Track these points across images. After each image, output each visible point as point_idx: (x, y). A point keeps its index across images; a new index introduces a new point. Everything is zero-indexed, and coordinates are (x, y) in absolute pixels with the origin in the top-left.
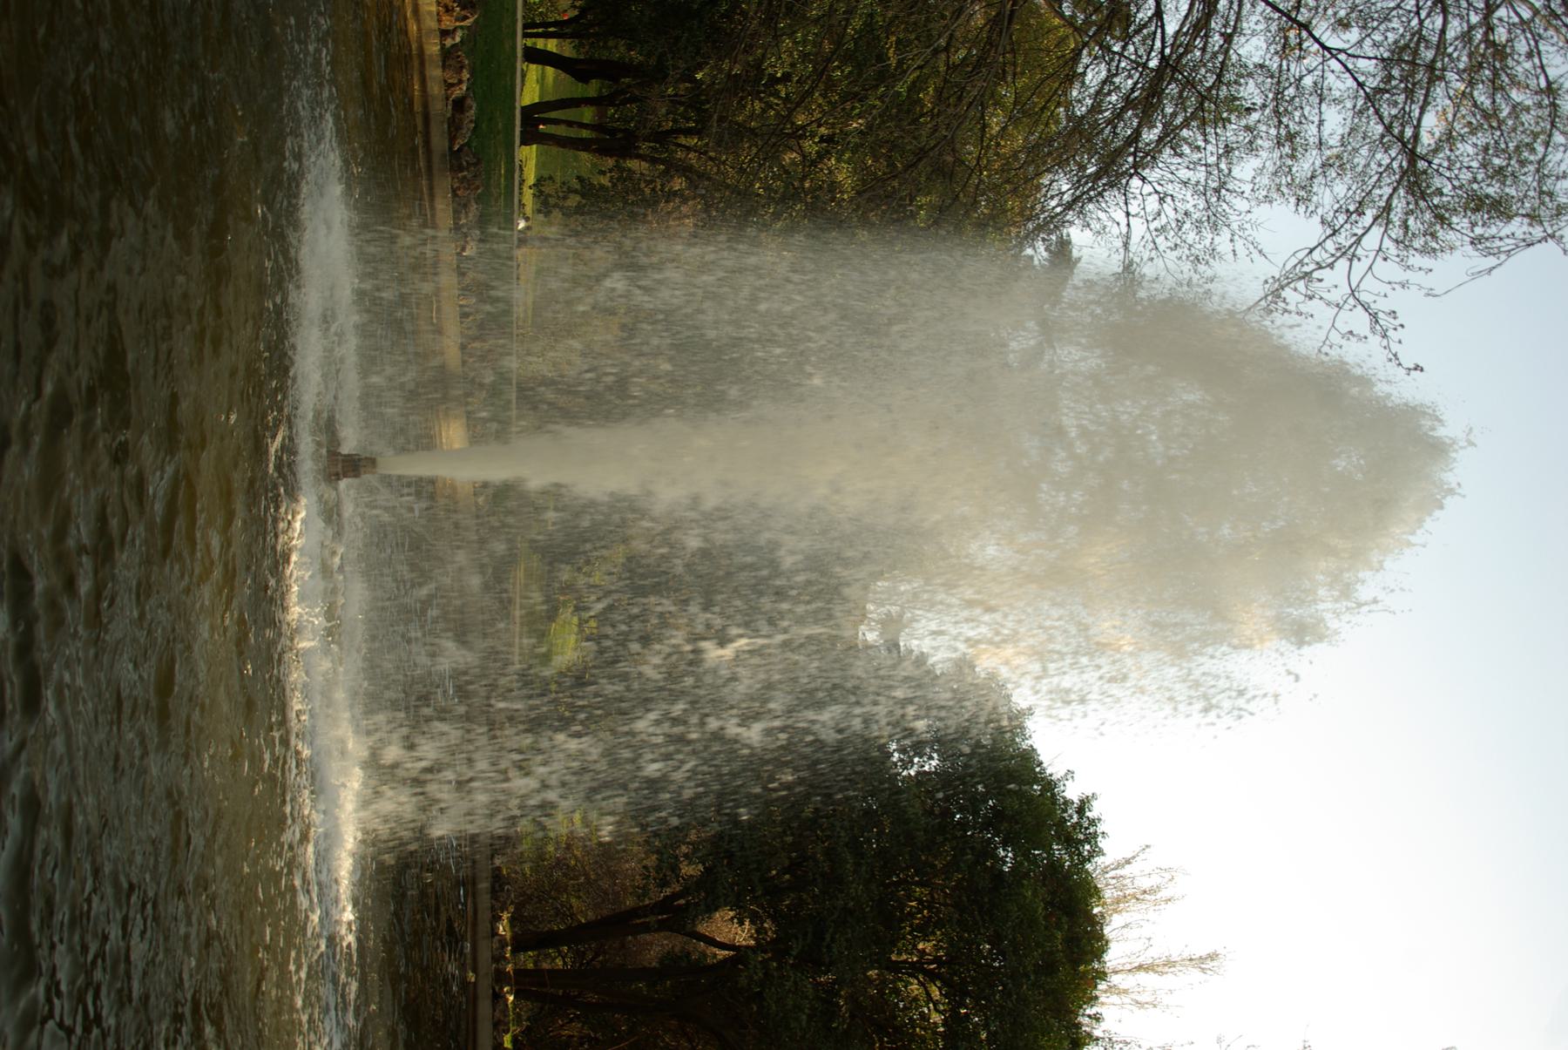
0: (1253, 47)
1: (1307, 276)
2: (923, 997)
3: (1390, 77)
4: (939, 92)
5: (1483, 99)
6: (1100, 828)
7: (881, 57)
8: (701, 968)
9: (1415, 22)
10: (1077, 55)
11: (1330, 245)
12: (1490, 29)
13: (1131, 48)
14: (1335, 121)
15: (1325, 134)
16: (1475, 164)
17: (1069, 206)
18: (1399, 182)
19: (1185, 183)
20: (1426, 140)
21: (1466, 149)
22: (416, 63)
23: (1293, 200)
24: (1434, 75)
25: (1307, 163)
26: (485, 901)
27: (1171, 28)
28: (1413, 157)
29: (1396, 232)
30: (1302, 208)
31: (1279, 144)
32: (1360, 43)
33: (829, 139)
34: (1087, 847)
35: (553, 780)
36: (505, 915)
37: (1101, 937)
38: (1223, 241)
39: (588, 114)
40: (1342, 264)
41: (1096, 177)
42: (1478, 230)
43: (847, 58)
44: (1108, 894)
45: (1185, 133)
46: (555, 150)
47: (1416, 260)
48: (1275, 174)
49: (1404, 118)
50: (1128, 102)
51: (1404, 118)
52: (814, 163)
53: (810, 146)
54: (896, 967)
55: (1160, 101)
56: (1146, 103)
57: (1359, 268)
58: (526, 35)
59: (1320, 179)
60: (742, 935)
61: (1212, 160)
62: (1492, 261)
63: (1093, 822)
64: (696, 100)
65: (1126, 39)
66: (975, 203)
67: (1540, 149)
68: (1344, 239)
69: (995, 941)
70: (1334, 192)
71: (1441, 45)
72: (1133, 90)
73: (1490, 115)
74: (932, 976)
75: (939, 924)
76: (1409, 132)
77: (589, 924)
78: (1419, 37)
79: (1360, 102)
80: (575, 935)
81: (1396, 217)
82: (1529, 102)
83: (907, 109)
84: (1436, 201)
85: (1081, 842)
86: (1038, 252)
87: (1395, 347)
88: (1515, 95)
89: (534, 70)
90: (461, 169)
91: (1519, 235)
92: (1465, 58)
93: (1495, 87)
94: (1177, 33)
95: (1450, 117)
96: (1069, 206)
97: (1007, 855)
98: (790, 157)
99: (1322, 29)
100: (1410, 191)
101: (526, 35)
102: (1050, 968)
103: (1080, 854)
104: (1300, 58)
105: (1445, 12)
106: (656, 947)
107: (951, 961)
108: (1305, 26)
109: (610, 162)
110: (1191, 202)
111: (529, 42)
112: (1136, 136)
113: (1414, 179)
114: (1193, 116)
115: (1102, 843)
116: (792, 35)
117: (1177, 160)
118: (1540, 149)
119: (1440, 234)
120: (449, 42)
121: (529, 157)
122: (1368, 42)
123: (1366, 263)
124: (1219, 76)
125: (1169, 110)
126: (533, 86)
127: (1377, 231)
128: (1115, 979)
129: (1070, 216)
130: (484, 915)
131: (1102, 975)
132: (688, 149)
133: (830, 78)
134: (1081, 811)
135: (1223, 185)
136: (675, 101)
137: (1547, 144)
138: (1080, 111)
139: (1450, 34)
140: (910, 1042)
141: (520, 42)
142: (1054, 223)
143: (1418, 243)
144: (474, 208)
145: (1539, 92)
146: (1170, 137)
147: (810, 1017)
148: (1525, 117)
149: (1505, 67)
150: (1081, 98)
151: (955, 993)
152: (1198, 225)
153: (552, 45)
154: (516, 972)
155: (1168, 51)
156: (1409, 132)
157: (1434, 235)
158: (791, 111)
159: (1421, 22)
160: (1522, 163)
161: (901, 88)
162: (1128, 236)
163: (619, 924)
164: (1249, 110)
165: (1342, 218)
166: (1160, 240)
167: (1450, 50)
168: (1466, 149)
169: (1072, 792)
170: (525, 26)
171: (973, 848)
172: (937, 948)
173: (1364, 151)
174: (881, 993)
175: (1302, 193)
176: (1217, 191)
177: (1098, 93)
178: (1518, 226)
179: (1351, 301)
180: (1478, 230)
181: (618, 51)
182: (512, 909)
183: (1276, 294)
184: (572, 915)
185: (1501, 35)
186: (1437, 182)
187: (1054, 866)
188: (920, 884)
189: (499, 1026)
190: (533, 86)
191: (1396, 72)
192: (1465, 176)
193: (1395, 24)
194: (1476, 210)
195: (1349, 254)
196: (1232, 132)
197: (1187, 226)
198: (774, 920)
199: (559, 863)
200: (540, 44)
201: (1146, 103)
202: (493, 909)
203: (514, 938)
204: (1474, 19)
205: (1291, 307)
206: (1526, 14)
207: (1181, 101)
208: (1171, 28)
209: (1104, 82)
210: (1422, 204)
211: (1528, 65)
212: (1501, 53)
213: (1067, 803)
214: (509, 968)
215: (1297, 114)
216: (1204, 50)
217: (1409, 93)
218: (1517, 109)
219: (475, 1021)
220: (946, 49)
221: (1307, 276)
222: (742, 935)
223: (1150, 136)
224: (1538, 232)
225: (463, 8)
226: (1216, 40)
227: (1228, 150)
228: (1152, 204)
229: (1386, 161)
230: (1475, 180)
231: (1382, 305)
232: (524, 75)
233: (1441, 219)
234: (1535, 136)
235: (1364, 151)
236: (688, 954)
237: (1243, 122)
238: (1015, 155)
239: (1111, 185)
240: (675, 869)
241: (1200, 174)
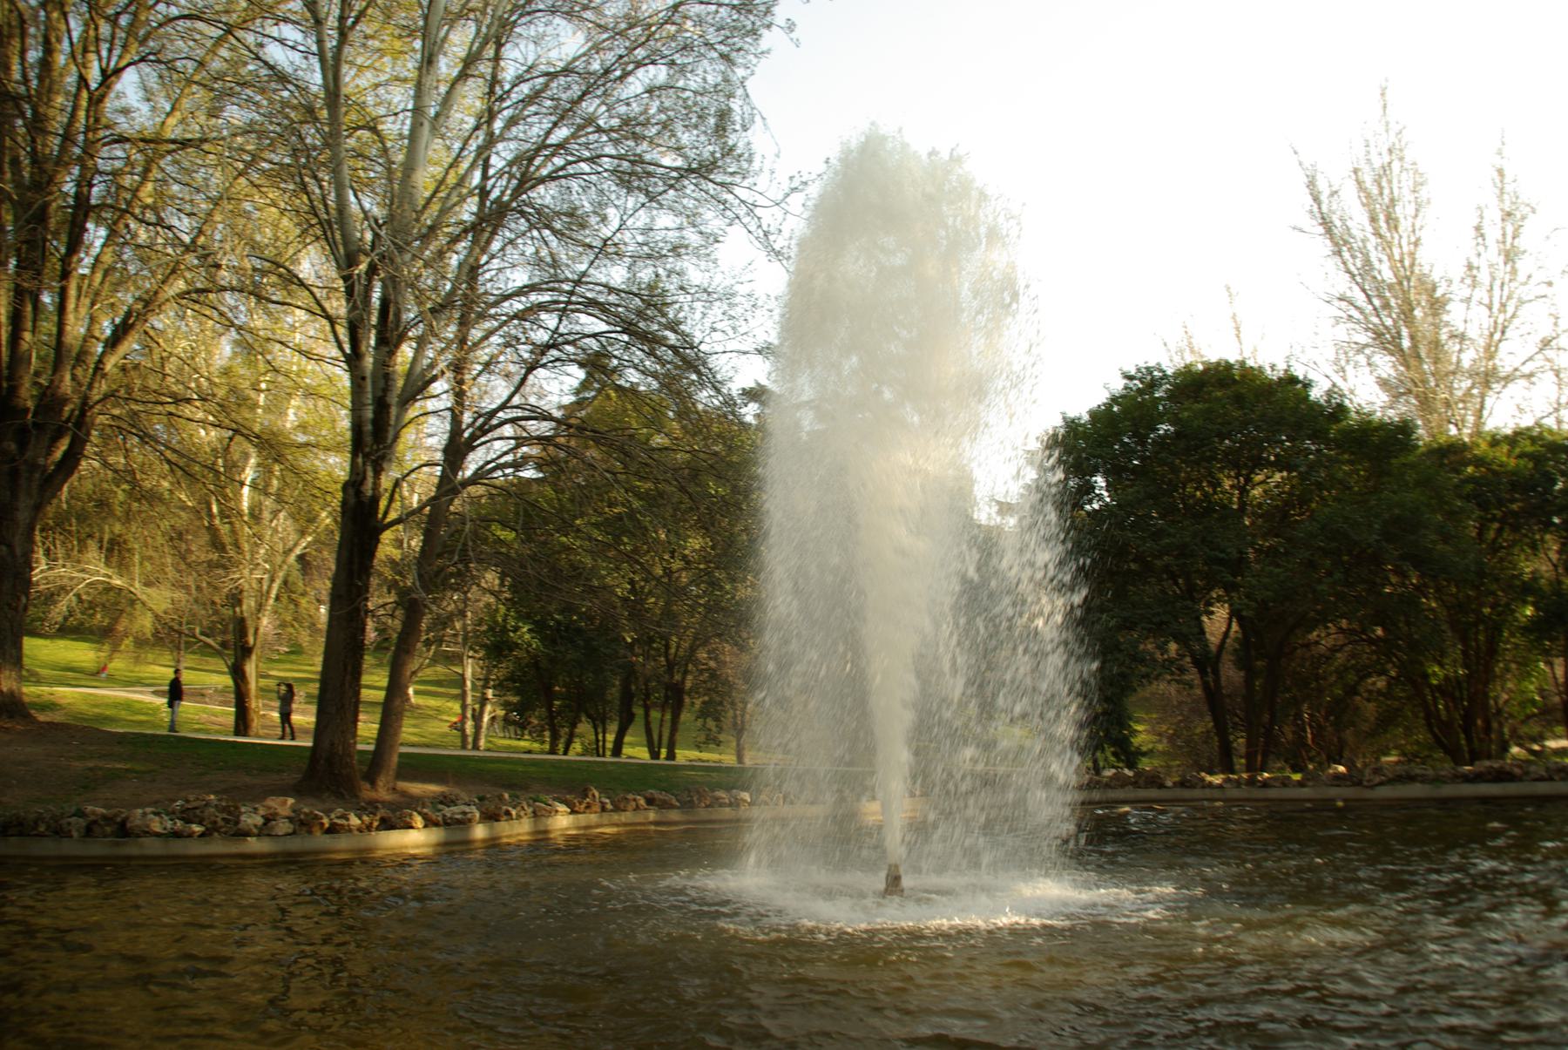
0: (616, 274)
1: (766, 234)
2: (1263, 486)
3: (639, 189)
4: (641, 478)
5: (654, 130)
6: (1142, 365)
7: (619, 517)
8: (1245, 642)
9: (605, 174)
10: (619, 388)
11: (746, 220)
12: (612, 130)
13: (616, 353)
14: (665, 220)
15: (674, 226)
16: (695, 132)
17: (718, 391)
18: (705, 178)
19: (704, 314)
20: (679, 163)
21: (686, 138)
22: (588, 832)
23: (716, 245)
24: (638, 160)
25: (692, 237)
26: (1197, 793)
27: (603, 327)
28: (690, 170)
29: (737, 179)
30: (721, 239)
31: (679, 255)
32: (616, 206)
33: (672, 553)
34: (1156, 373)
35: (1466, 292)
36: (1209, 778)
37: (1218, 364)
38: (742, 290)
39: (655, 715)
40: (758, 211)
41: (699, 373)
42: (738, 127)
43: (618, 540)
44: (1189, 359)
45: (671, 316)
46: (678, 737)
47: (756, 165)
48: (698, 257)
49: (663, 178)
50: (651, 353)
51: (663, 178)
52: (688, 562)
53: (677, 565)
54: (1242, 505)
55: (651, 333)
56: (651, 341)
57: (761, 201)
58: (604, 756)
59: (702, 228)
60: (1221, 612)
61: (689, 298)
62: (757, 118)
63: (1139, 370)
64: (646, 640)
65: (611, 356)
66: (715, 454)
67: (688, 94)
68: (742, 211)
69: (1222, 437)
70: (712, 219)
71: (620, 157)
72: (643, 350)
73: (665, 125)
74: (1248, 480)
75: (1211, 474)
76: (674, 174)
77: (1215, 719)
78: (614, 172)
79: (654, 204)
80: (1221, 730)
81: (729, 179)
82: (658, 103)
83: (653, 500)
84: (718, 155)
85: (1153, 377)
86: (749, 412)
87: (814, 176)
88: (652, 111)
89: (627, 750)
90: (691, 801)
91: (740, 103)
92: (629, 143)
93: (645, 124)
94: (608, 323)
95: (664, 149)
96: (718, 391)
97: (1164, 428)
98: (684, 578)
99: (606, 232)
100: (711, 171)
101: (604, 756)
102: (1239, 400)
103: (1162, 379)
104: (625, 244)
105: (599, 157)
106: (1230, 673)
107: (1236, 466)
108: (605, 241)
109: (687, 700)
110: (718, 309)
111: (608, 753)
112: (672, 347)
113: (702, 170)
114: (660, 311)
115: (1152, 364)
116: (604, 577)
117: (689, 321)
118: (688, 94)
119: (739, 152)
120: (609, 806)
121: (684, 755)
122: (616, 202)
123: (758, 197)
124: (636, 295)
125: (656, 327)
126: (635, 751)
127: (737, 190)
128: (1246, 355)
129: (725, 391)
130: (1208, 793)
131: (1242, 363)
132: (678, 647)
133: (632, 551)
134: (1131, 378)
135: (705, 291)
136: (647, 657)
137: (684, 89)
138: (655, 385)
139: (613, 152)
140: (1294, 495)
141: (609, 759)
142: (729, 402)
143: (745, 165)
144: (721, 794)
145: (651, 98)
146: (673, 326)
147: (1278, 566)
148: (667, 104)
149: (635, 118)
150: (647, 385)
151: (1259, 463)
152: (731, 305)
153: (610, 737)
154: (1248, 770)
155: (618, 329)
156: (674, 174)
157: (740, 156)
158: (655, 578)
159: (606, 170)
160: (695, 104)
161: (636, 504)
162: (738, 352)
163: (1213, 697)
164: (657, 276)
165: (728, 213)
166: (742, 330)
167: (623, 152)
168: (686, 138)
169: (1118, 385)
170: (598, 756)
171: (1158, 453)
172: (1229, 477)
173: (685, 201)
174: (1261, 516)
175: (712, 239)
176: (709, 294)
177: (643, 373)
178: (735, 104)
179: (783, 205)
180: (738, 127)
181: (614, 692)
182: (1203, 774)
183: (778, 253)
184: (1208, 732)
185: (615, 122)
186: (706, 155)
187: (1172, 396)
188: (1184, 488)
189: (1286, 783)
190: (635, 751)
191: (636, 184)
192: (703, 138)
193: (605, 186)
194: (724, 130)
195: (751, 208)
196: (671, 286)
197: (732, 313)
198: (1211, 589)
199: (1171, 739)
200: (609, 745)
201: (651, 341)
202: (1203, 787)
203: (1223, 773)
204: (605, 138)
205: (786, 243)
206: (604, 108)
207: (651, 319)
208: (603, 327)
209: (638, 370)
210: (720, 163)
211: (634, 105)
212: (626, 121)
213: (1126, 388)
214: (1245, 776)
215: (661, 245)
216: (618, 305)
217: (650, 174)
218: (661, 110)
219: (1281, 800)
220: (614, 474)
221: (766, 234)
222: (1221, 612)
223: (672, 338)
224: (740, 92)
225: (587, 796)
226: (612, 298)
227: (682, 288)
228: (717, 336)
229: (693, 187)
230: (705, 132)
231: (786, 186)
232: (630, 757)
233: (731, 150)
234: (678, 97)
235: (685, 201)
236: (1235, 650)
237: (664, 279)
238: (683, 427)
239: (705, 364)
240: (1171, 661)
241: (698, 305)
